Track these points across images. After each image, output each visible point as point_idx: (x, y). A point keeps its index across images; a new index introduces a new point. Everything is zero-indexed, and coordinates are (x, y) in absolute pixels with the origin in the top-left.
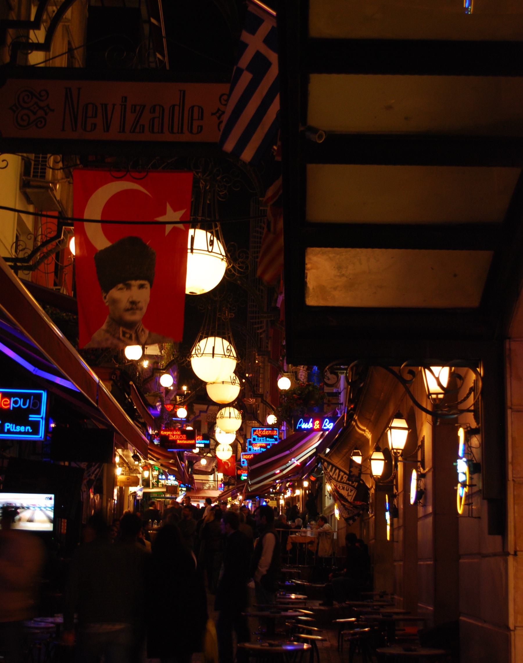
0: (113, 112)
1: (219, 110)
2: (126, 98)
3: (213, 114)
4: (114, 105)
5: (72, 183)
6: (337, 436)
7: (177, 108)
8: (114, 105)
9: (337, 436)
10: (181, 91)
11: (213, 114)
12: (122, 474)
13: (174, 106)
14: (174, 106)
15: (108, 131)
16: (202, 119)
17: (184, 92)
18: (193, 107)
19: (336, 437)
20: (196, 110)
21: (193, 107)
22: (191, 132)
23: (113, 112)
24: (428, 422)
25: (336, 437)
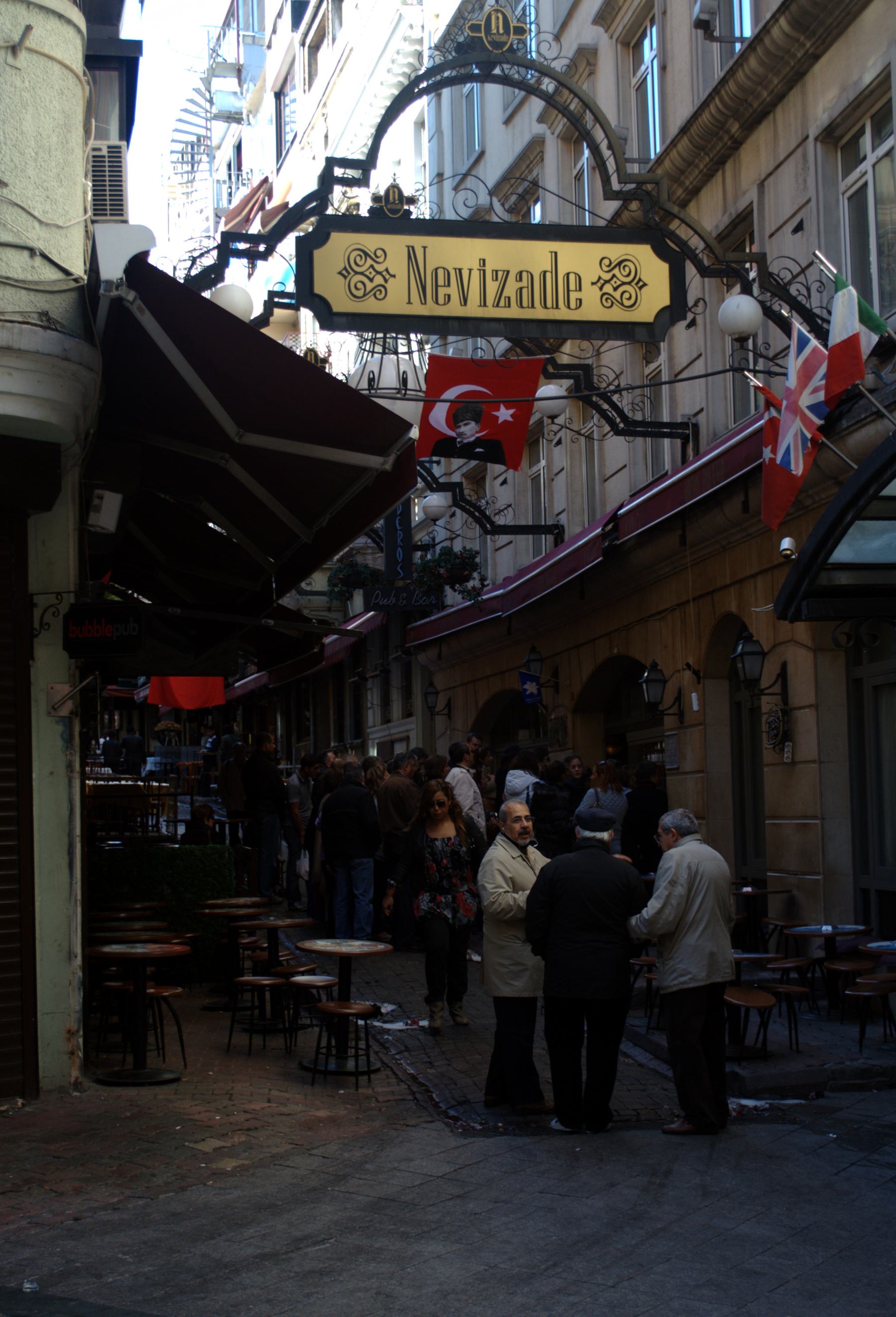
0: (785, 223)
1: (600, 278)
2: (484, 261)
3: (593, 284)
4: (470, 270)
5: (478, 348)
6: (665, 430)
7: (548, 275)
8: (470, 270)
9: (665, 430)
10: (552, 252)
11: (593, 284)
12: (738, 306)
13: (545, 272)
14: (545, 272)
15: (465, 304)
16: (580, 290)
17: (556, 253)
18: (568, 274)
19: (376, 803)
20: (572, 277)
21: (568, 274)
22: (546, 307)
23: (785, 223)
24: (295, 1045)
25: (376, 803)
